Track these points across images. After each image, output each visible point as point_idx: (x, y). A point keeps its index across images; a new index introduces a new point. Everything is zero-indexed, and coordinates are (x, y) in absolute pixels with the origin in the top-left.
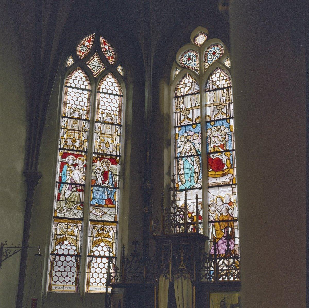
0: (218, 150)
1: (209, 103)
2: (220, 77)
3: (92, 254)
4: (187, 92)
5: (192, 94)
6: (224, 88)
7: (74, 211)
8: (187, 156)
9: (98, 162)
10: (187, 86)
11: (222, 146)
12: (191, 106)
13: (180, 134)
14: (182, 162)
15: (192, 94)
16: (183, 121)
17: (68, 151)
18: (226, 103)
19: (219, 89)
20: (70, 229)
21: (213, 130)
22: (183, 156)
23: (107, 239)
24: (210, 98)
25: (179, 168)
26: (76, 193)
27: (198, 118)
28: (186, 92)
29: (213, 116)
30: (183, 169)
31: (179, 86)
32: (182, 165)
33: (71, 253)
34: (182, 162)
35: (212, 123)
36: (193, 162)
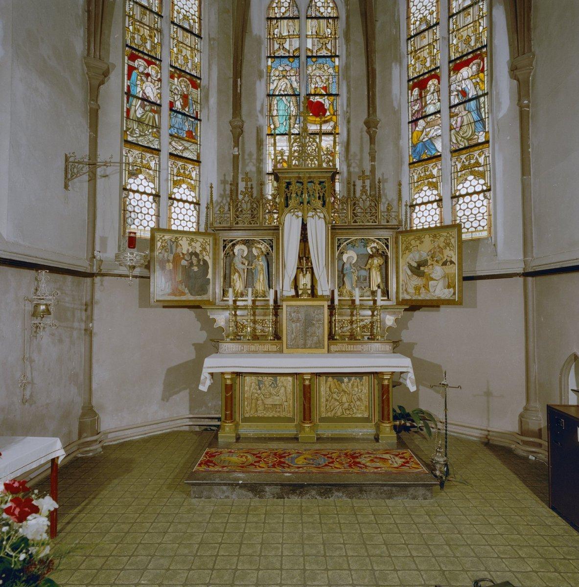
0: (320, 93)
1: (310, 33)
2: (325, 2)
3: (173, 196)
4: (283, 14)
5: (288, 18)
6: (330, 18)
7: (150, 137)
8: (282, 95)
9: (176, 79)
10: (283, 6)
11: (325, 88)
12: (287, 34)
13: (273, 66)
14: (275, 102)
15: (288, 18)
16: (277, 50)
17: (137, 53)
18: (331, 37)
19: (324, 18)
20: (145, 159)
21: (314, 68)
22: (277, 93)
23: (189, 180)
24: (312, 27)
25: (272, 108)
26: (151, 114)
27: (296, 50)
28: (282, 14)
29: (315, 51)
30: (277, 110)
31: (273, 5)
32: (275, 105)
33: (149, 191)
34: (275, 102)
35: (314, 59)
36: (290, 103)
